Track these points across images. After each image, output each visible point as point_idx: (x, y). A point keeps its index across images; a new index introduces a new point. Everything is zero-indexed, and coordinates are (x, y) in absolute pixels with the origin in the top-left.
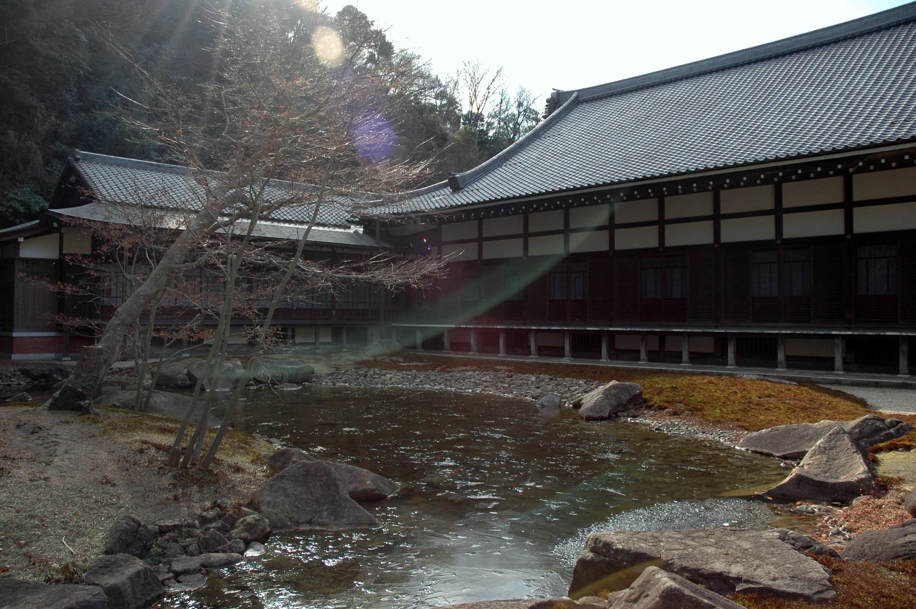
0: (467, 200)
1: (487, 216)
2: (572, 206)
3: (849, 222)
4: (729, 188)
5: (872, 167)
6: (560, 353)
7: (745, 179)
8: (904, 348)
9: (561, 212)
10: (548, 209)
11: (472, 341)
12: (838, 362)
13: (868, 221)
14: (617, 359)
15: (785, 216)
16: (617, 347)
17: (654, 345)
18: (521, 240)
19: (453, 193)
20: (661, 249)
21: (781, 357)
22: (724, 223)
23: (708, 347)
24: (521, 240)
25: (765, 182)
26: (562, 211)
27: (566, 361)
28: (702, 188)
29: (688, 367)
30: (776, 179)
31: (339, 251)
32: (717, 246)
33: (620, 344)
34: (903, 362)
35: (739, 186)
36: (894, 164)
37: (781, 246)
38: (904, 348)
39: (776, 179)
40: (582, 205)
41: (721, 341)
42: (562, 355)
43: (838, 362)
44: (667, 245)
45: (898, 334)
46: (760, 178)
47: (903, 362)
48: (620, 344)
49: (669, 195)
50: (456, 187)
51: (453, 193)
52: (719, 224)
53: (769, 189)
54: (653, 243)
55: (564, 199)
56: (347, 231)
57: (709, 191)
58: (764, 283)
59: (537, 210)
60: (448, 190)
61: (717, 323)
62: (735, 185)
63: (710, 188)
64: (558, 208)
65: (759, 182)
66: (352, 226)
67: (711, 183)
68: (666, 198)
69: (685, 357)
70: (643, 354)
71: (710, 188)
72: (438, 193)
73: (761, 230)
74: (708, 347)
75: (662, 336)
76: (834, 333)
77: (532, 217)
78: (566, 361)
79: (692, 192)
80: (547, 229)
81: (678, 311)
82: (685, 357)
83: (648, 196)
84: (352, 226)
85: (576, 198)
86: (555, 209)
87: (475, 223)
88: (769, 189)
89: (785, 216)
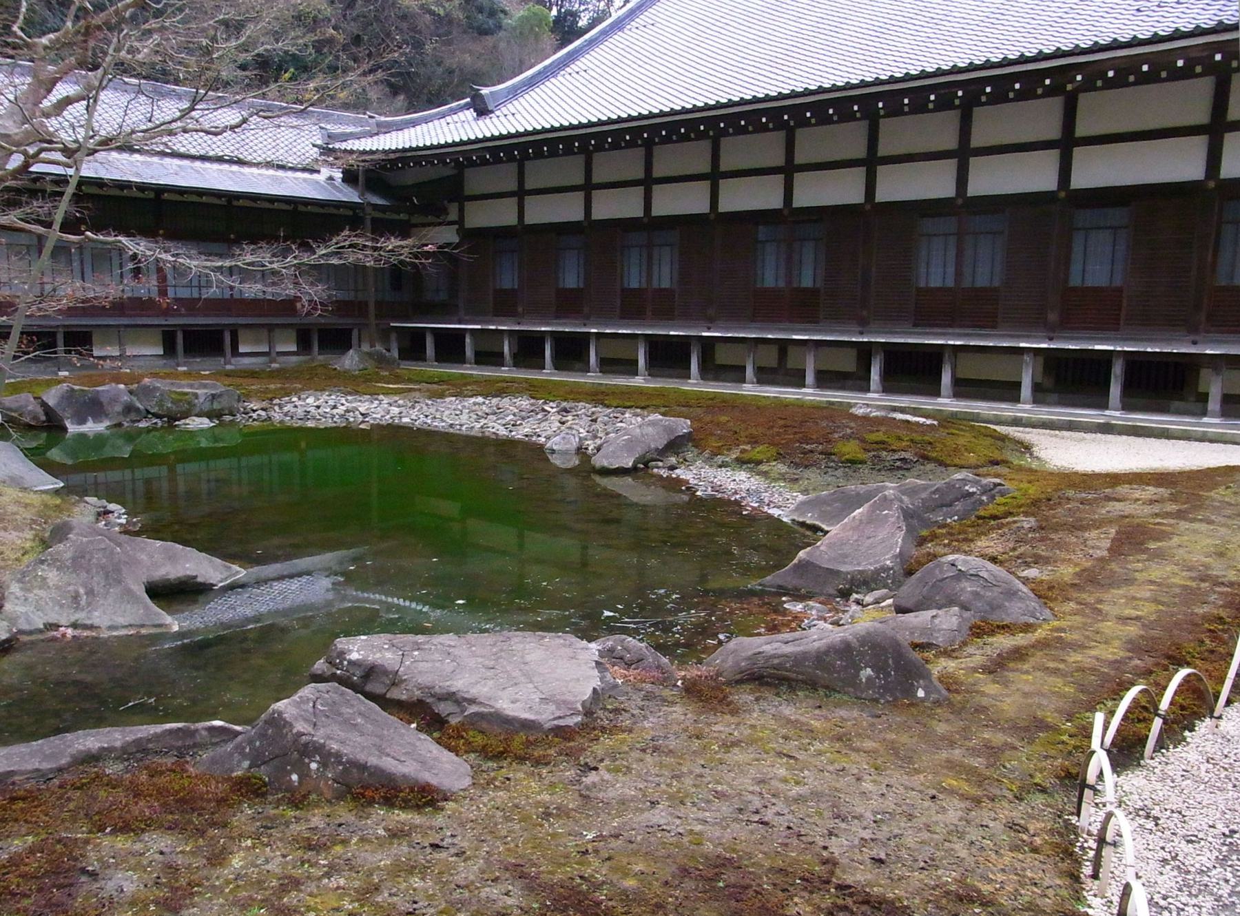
0: (717, 98)
1: (599, 148)
2: (724, 133)
3: (962, 180)
4: (935, 110)
5: (1164, 74)
6: (629, 367)
7: (988, 90)
8: (1117, 369)
9: (705, 145)
10: (685, 138)
11: (506, 349)
12: (1026, 391)
13: (1096, 170)
14: (716, 379)
15: (972, 160)
16: (718, 362)
17: (770, 358)
18: (580, 195)
19: (476, 120)
20: (586, 224)
21: (946, 379)
22: (529, 200)
23: (848, 363)
24: (580, 195)
25: (1050, 92)
26: (515, 164)
27: (638, 381)
28: (944, 104)
29: (599, 378)
30: (1069, 87)
31: (301, 208)
32: (1062, 194)
33: (723, 356)
34: (1115, 390)
35: (1006, 100)
36: (1199, 69)
37: (963, 209)
38: (1117, 369)
39: (1069, 87)
40: (743, 131)
41: (865, 353)
42: (634, 373)
43: (1026, 391)
44: (721, 210)
45: (1111, 348)
46: (1014, 90)
47: (1115, 390)
48: (723, 356)
49: (887, 115)
50: (482, 111)
51: (476, 120)
52: (968, 164)
53: (1055, 105)
54: (577, 215)
55: (712, 122)
56: (315, 176)
57: (956, 108)
58: (936, 270)
59: (667, 140)
60: (470, 114)
61: (864, 325)
62: (999, 97)
63: (957, 102)
64: (701, 136)
65: (1011, 95)
66: (323, 170)
67: (960, 93)
68: (881, 120)
69: (810, 378)
70: (749, 372)
71: (957, 102)
72: (455, 117)
73: (935, 183)
74: (848, 363)
75: (783, 345)
76: (1022, 345)
77: (598, 158)
78: (638, 381)
79: (558, 155)
80: (837, 157)
81: (804, 307)
82: (810, 378)
83: (851, 117)
84: (323, 170)
85: (732, 119)
86: (697, 139)
87: (580, 160)
88: (1055, 105)
89: (972, 160)
